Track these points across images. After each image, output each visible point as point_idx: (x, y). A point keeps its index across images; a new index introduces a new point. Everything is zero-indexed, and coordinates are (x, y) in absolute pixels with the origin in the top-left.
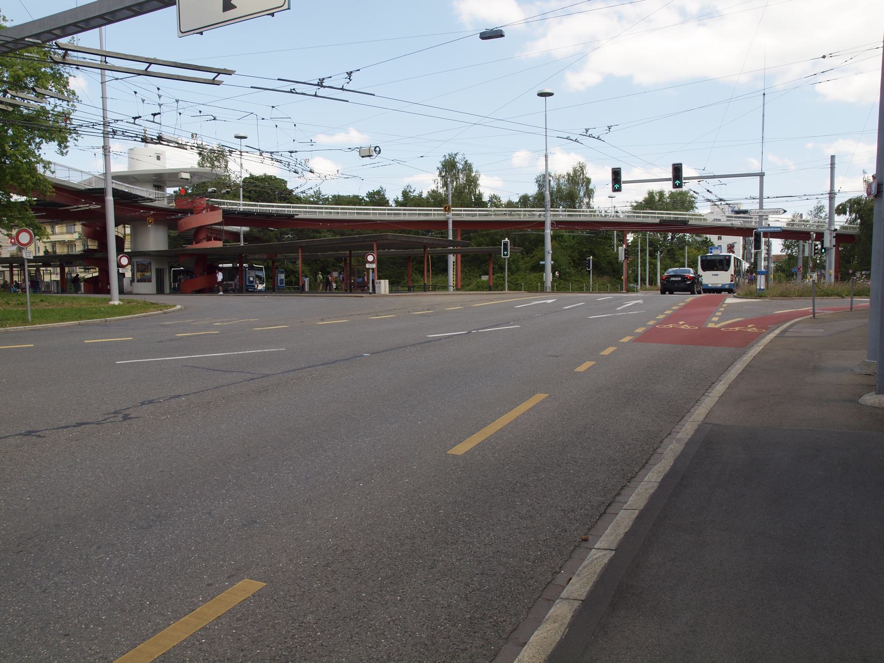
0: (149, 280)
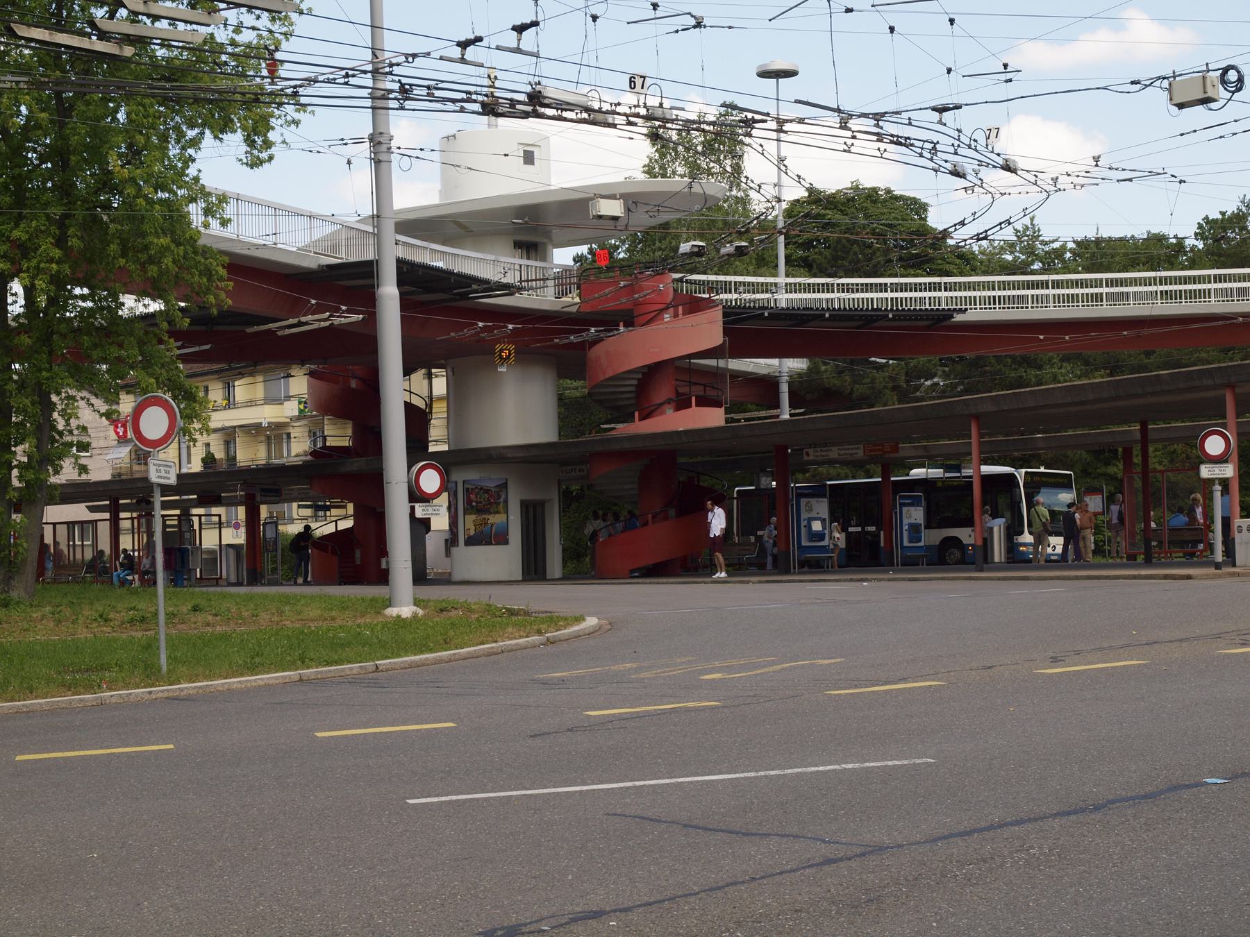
0: (501, 538)
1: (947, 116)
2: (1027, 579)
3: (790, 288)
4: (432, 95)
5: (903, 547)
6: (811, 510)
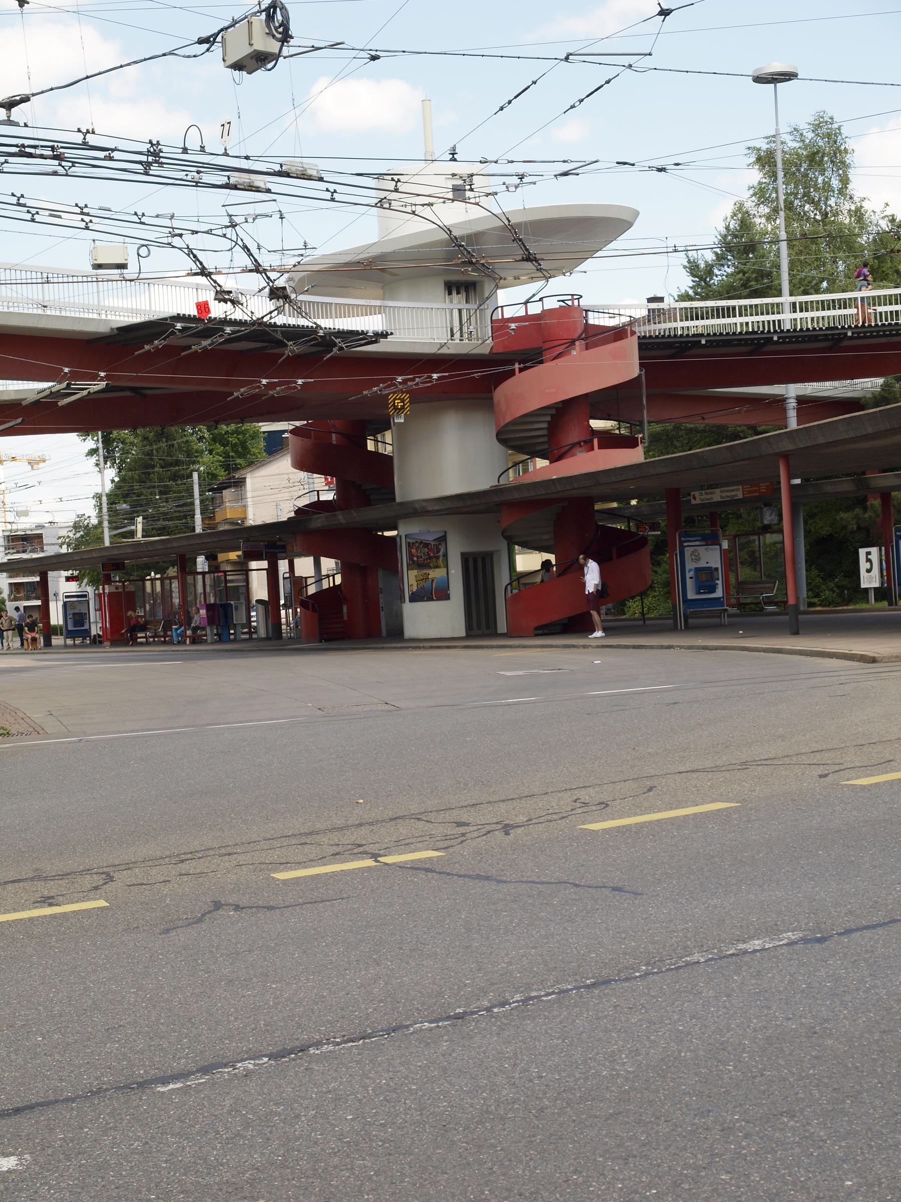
0: (442, 594)
4: (53, 148)
5: (686, 601)
6: (698, 559)
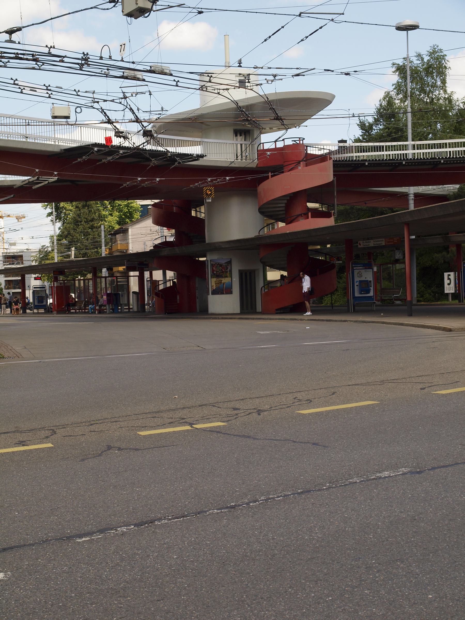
1: (15, 37)
2: (296, 319)
3: (414, 147)
5: (354, 297)
